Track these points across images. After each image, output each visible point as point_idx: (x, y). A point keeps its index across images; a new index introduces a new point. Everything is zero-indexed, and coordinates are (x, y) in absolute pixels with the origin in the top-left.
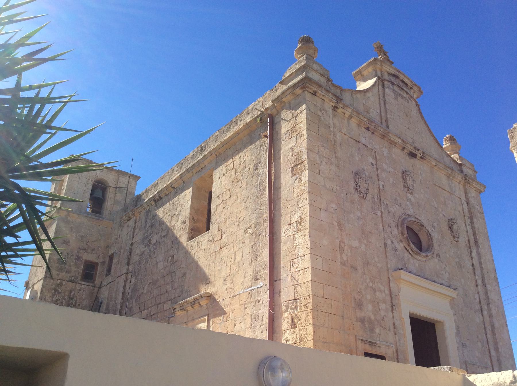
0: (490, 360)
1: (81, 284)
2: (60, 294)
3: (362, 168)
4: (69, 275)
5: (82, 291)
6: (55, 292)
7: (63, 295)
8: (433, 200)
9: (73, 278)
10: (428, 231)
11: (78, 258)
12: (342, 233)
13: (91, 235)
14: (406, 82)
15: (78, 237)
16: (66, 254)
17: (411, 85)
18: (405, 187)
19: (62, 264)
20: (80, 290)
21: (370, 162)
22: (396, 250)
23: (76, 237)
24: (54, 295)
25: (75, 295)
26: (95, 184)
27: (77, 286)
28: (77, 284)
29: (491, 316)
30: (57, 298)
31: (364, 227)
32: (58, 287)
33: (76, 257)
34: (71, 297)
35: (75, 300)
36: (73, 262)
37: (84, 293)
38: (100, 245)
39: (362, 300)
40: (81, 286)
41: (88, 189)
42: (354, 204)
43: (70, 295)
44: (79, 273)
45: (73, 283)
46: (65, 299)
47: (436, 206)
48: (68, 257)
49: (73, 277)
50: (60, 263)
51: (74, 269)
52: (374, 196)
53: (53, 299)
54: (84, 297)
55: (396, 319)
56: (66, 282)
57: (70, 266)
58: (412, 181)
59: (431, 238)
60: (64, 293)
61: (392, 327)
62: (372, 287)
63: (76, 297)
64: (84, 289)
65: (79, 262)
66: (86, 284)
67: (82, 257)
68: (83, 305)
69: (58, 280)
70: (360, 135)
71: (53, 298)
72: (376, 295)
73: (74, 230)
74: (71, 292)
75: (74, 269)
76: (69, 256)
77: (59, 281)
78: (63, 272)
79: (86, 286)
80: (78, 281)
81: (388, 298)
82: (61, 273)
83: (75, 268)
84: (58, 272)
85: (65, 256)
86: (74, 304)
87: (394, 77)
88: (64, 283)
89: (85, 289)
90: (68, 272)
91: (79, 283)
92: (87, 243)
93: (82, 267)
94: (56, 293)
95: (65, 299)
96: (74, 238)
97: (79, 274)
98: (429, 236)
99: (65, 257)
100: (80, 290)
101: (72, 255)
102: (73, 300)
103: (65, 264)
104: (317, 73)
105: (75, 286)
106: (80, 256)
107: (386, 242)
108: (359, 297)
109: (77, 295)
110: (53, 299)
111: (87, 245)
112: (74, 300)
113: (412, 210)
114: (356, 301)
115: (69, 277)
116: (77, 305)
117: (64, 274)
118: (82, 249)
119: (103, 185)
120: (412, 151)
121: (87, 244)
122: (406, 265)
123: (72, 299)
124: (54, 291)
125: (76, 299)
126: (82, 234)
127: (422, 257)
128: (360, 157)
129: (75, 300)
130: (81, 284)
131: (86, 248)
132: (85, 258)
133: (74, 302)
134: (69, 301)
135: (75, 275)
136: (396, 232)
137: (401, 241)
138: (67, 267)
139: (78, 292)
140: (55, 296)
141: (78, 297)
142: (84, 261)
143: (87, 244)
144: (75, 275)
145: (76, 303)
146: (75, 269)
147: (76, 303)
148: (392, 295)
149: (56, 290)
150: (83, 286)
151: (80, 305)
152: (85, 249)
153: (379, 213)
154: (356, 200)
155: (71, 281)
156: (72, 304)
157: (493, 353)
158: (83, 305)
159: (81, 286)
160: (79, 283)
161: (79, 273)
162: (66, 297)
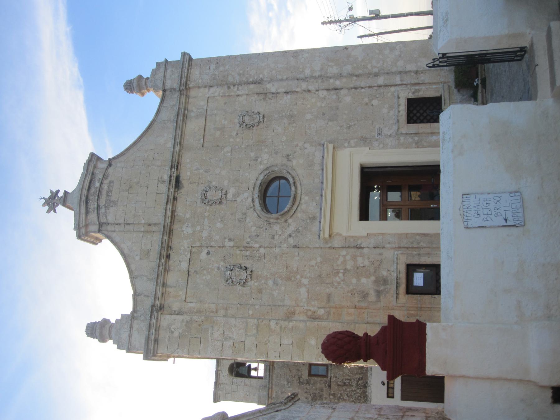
0: (390, 87)
1: (331, 377)
2: (342, 394)
3: (218, 271)
4: (324, 389)
5: (337, 375)
6: (341, 399)
7: (342, 392)
8: (223, 152)
9: (326, 385)
10: (265, 175)
11: (308, 383)
12: (297, 312)
13: (285, 374)
14: (88, 184)
15: (289, 385)
16: (307, 394)
17: (89, 175)
18: (220, 203)
19: (316, 396)
20: (336, 377)
21: (206, 256)
22: (297, 231)
23: (289, 387)
24: (344, 400)
25: (341, 381)
26: (235, 374)
27: (333, 380)
28: (331, 380)
29: (340, 76)
30: (346, 396)
31: (283, 277)
32: (337, 397)
33: (308, 385)
34: (343, 384)
35: (345, 380)
36: (312, 387)
37: (338, 373)
38: (293, 365)
39: (359, 291)
40: (333, 377)
41: (242, 382)
42: (261, 289)
43: (342, 385)
44: (322, 380)
45: (331, 384)
46: (346, 389)
47: (229, 149)
48: (309, 392)
49: (325, 385)
50: (315, 398)
51: (318, 385)
52: (244, 256)
53: (347, 399)
54: (341, 373)
55: (370, 244)
56: (331, 390)
57: (316, 389)
58: (210, 190)
59: (272, 172)
60: (341, 391)
61: (378, 251)
62: (344, 274)
63: (343, 380)
64: (334, 374)
65: (312, 381)
66: (330, 373)
67: (307, 380)
68: (349, 373)
69: (331, 397)
70: (180, 270)
71: (346, 400)
72: (351, 269)
73: (284, 390)
74: (339, 385)
75: (318, 385)
76: (308, 391)
77: (331, 397)
78: (323, 394)
79: (332, 373)
80: (328, 380)
81: (350, 250)
82: (324, 397)
83: (317, 384)
84: (324, 399)
85: (308, 394)
86: (349, 381)
87: (88, 203)
88: (333, 392)
89: (335, 373)
90: (322, 390)
91: (330, 379)
92: (293, 376)
93: (315, 378)
94: (342, 397)
95: (346, 389)
96: (291, 389)
97: (322, 380)
98: (270, 174)
99: (309, 395)
100: (336, 377)
101: (307, 389)
102: (346, 383)
103: (315, 393)
104: (132, 335)
105: (333, 382)
106: (306, 382)
107: (292, 245)
108: (356, 295)
109: (341, 379)
110: (347, 399)
111: (295, 376)
112: (345, 382)
113: (246, 195)
114: (361, 300)
115: (326, 389)
116: (349, 378)
117: (324, 393)
118: (299, 381)
119: (234, 366)
120: (174, 186)
121: (294, 377)
122: (310, 217)
123: (345, 383)
124: (340, 400)
125: (344, 380)
126: (286, 383)
127: (297, 190)
128: (205, 272)
129: (345, 380)
130: (331, 377)
131: (298, 377)
132: (307, 377)
133: (347, 381)
134: (347, 385)
135: (324, 383)
136: (277, 228)
137: (286, 221)
138: (317, 392)
139: (338, 378)
140: (345, 398)
141: (343, 378)
142: (310, 378)
143: (294, 377)
144: (324, 383)
145: (348, 379)
146: (319, 384)
147: (348, 379)
148: (346, 246)
149: (340, 398)
150: (332, 375)
151: (349, 375)
152: (299, 378)
153: (262, 251)
154: (256, 284)
155: (330, 386)
156: (349, 383)
157: (381, 81)
158: (349, 373)
159: (333, 377)
160: (330, 379)
161: (322, 380)
162: (344, 389)
